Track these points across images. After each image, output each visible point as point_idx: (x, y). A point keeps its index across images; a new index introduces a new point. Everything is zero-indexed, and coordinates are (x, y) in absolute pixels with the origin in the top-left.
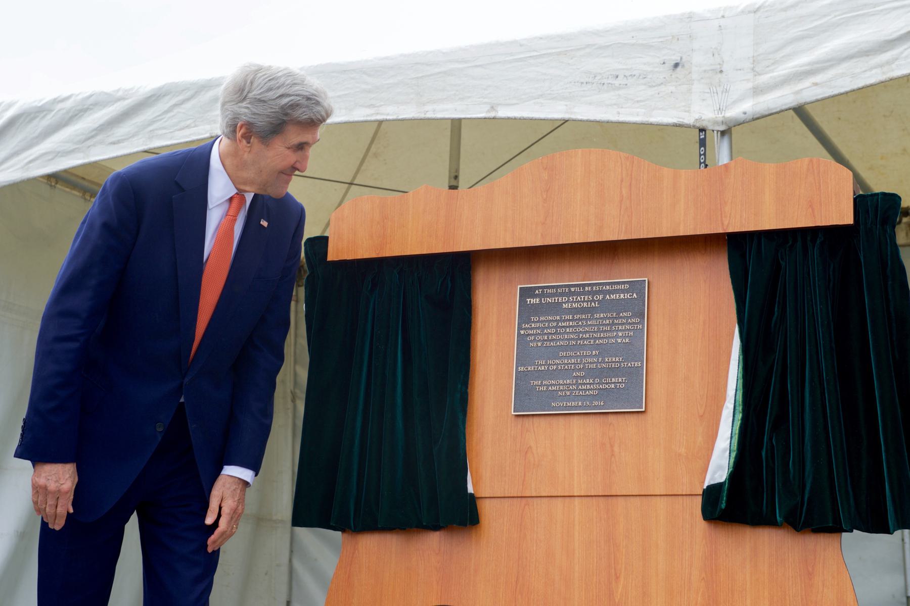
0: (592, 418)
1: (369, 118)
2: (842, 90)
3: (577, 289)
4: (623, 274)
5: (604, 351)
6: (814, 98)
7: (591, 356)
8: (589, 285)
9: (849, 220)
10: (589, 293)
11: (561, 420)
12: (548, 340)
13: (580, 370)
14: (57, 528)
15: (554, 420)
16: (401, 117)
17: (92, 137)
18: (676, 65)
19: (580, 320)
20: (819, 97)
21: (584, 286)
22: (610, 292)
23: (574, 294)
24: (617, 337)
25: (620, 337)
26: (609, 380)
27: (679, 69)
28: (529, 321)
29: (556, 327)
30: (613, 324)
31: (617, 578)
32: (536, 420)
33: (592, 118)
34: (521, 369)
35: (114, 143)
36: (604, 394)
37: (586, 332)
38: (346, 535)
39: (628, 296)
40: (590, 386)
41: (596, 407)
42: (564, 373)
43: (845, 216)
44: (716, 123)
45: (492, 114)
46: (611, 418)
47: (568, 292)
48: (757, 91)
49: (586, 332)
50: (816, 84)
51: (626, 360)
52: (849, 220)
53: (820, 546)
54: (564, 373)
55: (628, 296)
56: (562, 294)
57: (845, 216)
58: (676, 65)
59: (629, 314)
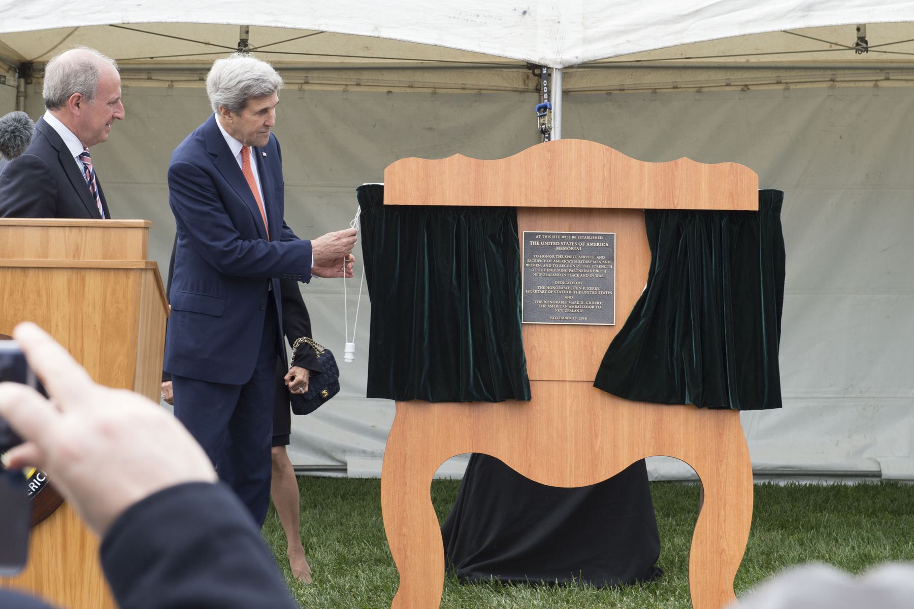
0: (578, 329)
1: (269, 24)
2: (647, 49)
3: (566, 237)
4: (599, 228)
5: (587, 282)
6: (627, 52)
7: (578, 285)
8: (575, 235)
9: (755, 207)
10: (574, 240)
11: (556, 328)
12: (546, 272)
13: (569, 295)
14: (384, 445)
15: (551, 328)
16: (297, 27)
17: (6, 10)
18: (525, 13)
19: (569, 259)
20: (631, 51)
21: (571, 235)
22: (589, 241)
23: (564, 240)
24: (595, 273)
25: (597, 273)
26: (590, 303)
27: (527, 15)
28: (532, 258)
29: (552, 263)
30: (592, 264)
31: (596, 436)
32: (538, 327)
33: (459, 47)
34: (528, 291)
35: (28, 18)
36: (587, 312)
37: (573, 268)
38: (403, 404)
39: (602, 244)
40: (577, 306)
41: (581, 321)
42: (560, 296)
43: (753, 205)
44: (556, 63)
45: (376, 34)
46: (591, 329)
47: (560, 238)
48: (587, 41)
49: (573, 268)
50: (629, 41)
51: (601, 289)
52: (755, 207)
53: (726, 416)
54: (560, 296)
55: (602, 244)
56: (555, 240)
57: (753, 205)
58: (525, 13)
59: (603, 257)
